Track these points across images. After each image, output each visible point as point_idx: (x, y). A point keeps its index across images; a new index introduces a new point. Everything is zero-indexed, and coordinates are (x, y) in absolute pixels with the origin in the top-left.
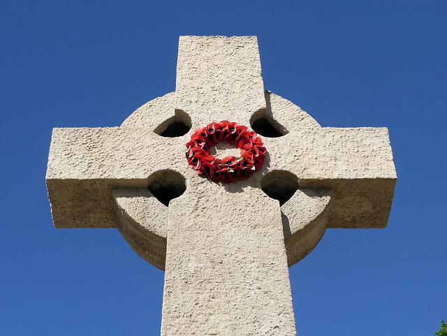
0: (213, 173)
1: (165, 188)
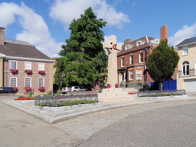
0: (114, 48)
1: (111, 49)
